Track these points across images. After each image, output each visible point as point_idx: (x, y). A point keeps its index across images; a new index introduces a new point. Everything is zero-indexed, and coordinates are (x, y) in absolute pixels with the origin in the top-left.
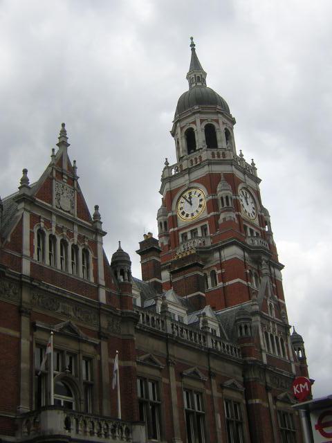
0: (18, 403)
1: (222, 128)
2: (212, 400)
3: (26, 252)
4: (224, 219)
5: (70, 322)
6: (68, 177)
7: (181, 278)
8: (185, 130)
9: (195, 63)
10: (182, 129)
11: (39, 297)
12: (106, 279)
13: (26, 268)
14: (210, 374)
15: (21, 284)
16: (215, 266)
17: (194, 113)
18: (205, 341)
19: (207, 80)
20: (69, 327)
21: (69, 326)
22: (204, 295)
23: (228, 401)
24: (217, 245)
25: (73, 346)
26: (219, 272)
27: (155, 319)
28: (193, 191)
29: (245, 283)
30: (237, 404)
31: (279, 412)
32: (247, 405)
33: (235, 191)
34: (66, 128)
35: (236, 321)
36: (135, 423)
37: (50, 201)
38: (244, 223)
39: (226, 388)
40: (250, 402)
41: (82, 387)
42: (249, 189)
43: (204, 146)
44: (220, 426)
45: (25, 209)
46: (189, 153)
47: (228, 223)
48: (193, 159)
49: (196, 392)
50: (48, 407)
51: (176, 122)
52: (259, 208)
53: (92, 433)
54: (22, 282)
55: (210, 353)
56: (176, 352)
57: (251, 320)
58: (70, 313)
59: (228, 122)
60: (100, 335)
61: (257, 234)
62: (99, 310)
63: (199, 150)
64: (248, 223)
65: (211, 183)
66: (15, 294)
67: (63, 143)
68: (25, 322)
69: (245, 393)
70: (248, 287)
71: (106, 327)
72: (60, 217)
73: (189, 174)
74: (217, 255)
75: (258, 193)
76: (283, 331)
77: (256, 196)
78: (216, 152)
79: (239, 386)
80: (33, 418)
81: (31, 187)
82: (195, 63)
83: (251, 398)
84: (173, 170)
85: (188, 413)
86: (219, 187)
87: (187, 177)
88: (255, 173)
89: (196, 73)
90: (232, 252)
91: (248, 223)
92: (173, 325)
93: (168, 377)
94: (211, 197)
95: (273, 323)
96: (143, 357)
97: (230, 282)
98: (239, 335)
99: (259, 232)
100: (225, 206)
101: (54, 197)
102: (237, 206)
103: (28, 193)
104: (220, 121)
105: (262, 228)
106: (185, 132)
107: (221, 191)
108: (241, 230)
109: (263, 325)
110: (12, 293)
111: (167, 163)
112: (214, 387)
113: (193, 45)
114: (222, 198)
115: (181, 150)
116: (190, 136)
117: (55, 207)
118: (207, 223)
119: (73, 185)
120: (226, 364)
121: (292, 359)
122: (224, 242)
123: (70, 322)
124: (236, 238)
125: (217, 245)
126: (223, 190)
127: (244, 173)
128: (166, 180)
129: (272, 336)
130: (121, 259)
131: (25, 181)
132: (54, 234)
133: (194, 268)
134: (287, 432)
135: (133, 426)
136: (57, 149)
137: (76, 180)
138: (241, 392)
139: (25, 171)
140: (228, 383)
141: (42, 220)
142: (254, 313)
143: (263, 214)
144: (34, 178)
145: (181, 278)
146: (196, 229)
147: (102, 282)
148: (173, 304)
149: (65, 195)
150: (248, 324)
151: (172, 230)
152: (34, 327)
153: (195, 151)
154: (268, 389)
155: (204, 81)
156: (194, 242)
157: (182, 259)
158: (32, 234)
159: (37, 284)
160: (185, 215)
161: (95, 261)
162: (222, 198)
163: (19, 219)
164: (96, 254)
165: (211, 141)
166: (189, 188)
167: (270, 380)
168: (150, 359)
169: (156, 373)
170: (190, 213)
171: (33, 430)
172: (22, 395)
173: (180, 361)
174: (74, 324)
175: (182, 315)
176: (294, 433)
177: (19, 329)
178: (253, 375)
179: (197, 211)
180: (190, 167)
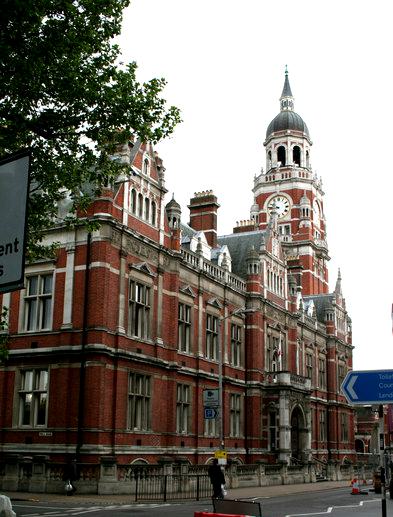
2: (119, 281)
3: (266, 285)
28: (281, 198)
30: (239, 327)
49: (138, 284)
65: (296, 195)
74: (295, 250)
77: (321, 206)
86: (302, 201)
126: (305, 204)
130: (172, 207)
150: (177, 217)
152: (268, 326)
178: (256, 306)
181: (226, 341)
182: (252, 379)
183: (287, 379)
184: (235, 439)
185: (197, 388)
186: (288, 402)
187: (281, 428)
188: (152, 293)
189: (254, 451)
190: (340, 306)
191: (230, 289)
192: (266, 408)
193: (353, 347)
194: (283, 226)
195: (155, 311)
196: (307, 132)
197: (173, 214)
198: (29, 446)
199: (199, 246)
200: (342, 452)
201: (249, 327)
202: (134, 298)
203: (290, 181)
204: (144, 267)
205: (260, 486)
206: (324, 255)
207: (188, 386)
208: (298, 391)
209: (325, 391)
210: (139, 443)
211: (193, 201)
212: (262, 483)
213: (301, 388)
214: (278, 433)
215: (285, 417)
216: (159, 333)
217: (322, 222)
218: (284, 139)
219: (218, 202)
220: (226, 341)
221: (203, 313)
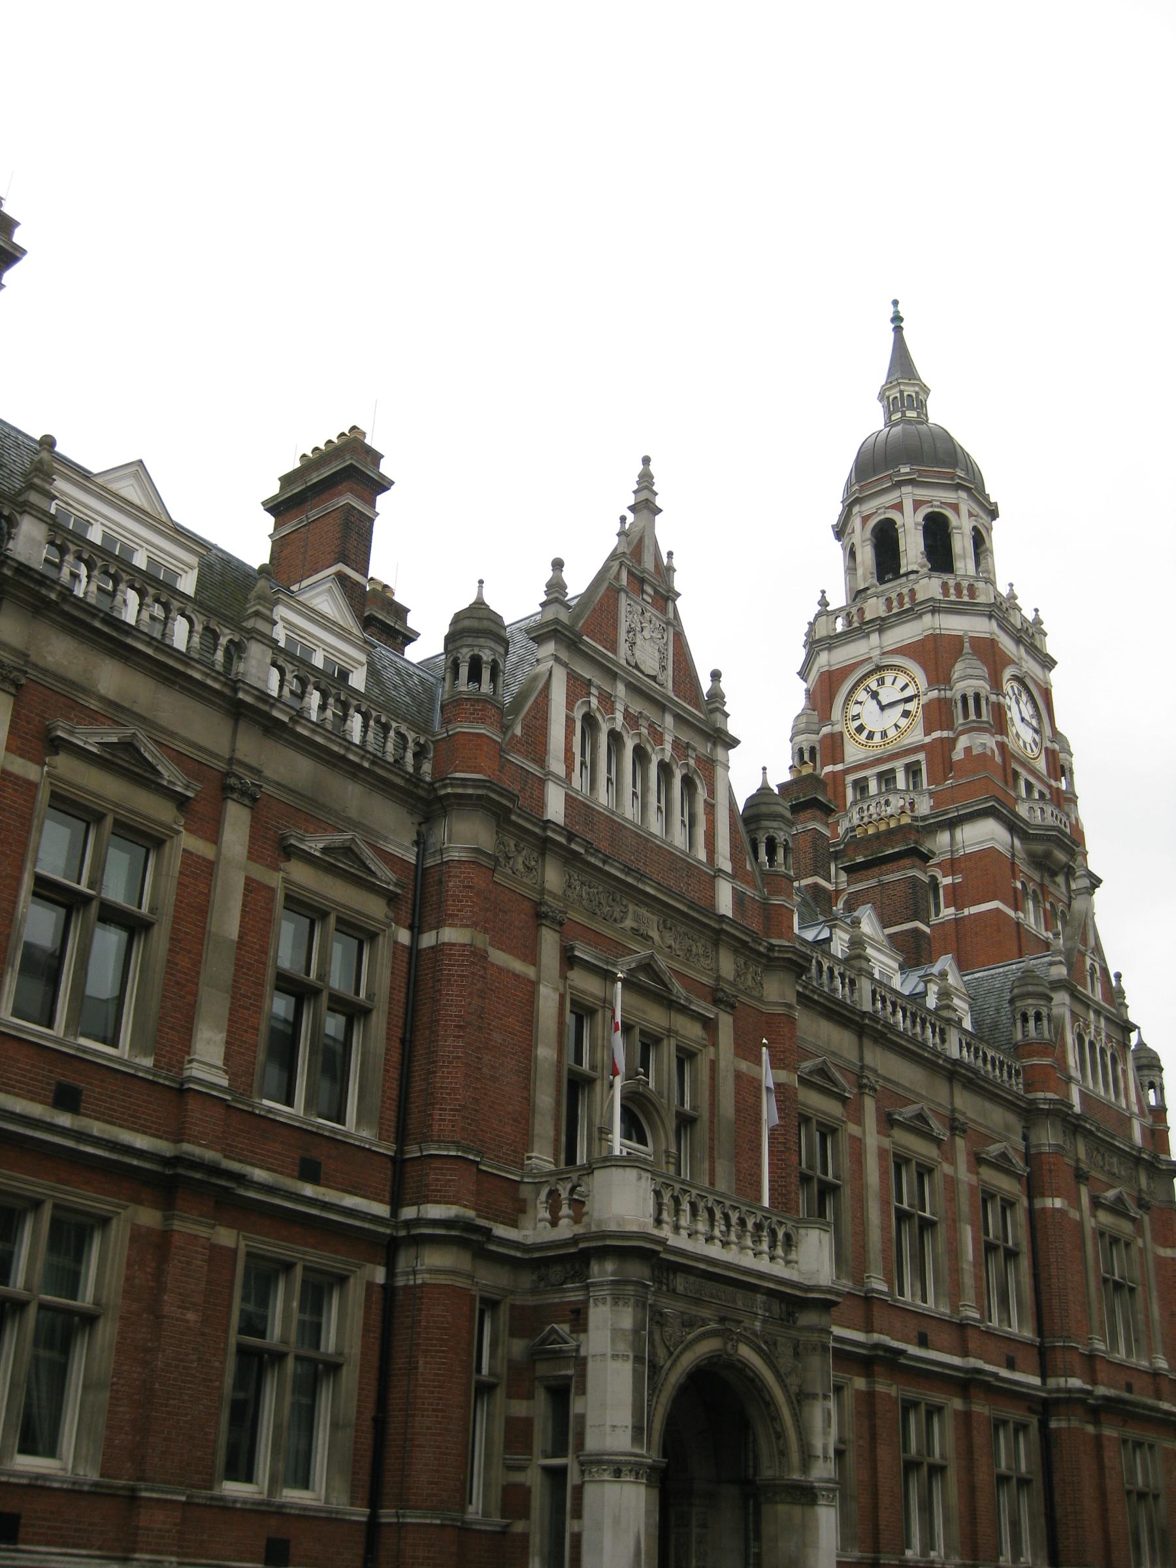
0: (527, 1146)
3: (557, 766)
4: (968, 750)
5: (652, 956)
6: (656, 591)
7: (873, 882)
8: (872, 523)
10: (865, 520)
11: (583, 883)
12: (733, 859)
13: (555, 808)
14: (956, 1126)
15: (544, 846)
16: (938, 865)
17: (899, 485)
19: (931, 404)
21: (649, 965)
22: (927, 930)
24: (946, 812)
25: (655, 1017)
26: (948, 880)
27: (836, 973)
28: (889, 677)
29: (1011, 913)
30: (1008, 1204)
31: (1102, 1234)
32: (1031, 1212)
33: (996, 685)
34: (653, 468)
35: (1012, 1001)
36: (800, 1223)
37: (613, 647)
38: (1015, 766)
40: (428, 940)
41: (671, 1124)
42: (1028, 681)
43: (922, 566)
44: (970, 1257)
45: (557, 659)
46: (881, 580)
48: (894, 596)
50: (610, 1162)
51: (851, 503)
52: (1048, 731)
53: (710, 1239)
54: (548, 840)
55: (953, 1073)
56: (879, 1060)
57: (1052, 999)
58: (651, 933)
59: (982, 514)
60: (717, 998)
61: (1042, 795)
62: (716, 933)
63: (907, 574)
64: (1024, 765)
65: (936, 656)
66: (529, 869)
67: (645, 505)
68: (549, 942)
69: (1028, 1178)
70: (1018, 924)
71: (731, 978)
72: (635, 689)
73: (881, 631)
74: (944, 838)
75: (1047, 694)
76: (1117, 1035)
78: (952, 583)
79: (1018, 1161)
80: (569, 1186)
81: (573, 603)
83: (1043, 1195)
84: (840, 621)
86: (959, 669)
87: (874, 638)
88: (1043, 642)
89: (903, 382)
90: (983, 834)
91: (1024, 765)
92: (874, 992)
93: (859, 1122)
94: (934, 694)
95: (1098, 1013)
96: (807, 1065)
97: (974, 910)
98: (1019, 1036)
99: (1046, 792)
100: (973, 717)
101: (623, 635)
102: (1000, 723)
103: (564, 617)
104: (964, 509)
105: (1053, 783)
106: (880, 521)
107: (963, 678)
108: (1006, 783)
109: (1075, 1016)
110: (520, 867)
111: (824, 603)
112: (962, 1158)
113: (897, 319)
114: (964, 698)
115: (860, 572)
116: (886, 540)
117: (623, 662)
118: (921, 756)
119: (664, 611)
120: (988, 1105)
121: (1135, 1109)
122: (965, 807)
123: (652, 956)
124: (998, 800)
125: (946, 812)
126: (968, 679)
127: (1018, 641)
128: (815, 644)
129: (1092, 1044)
131: (556, 587)
132: (618, 729)
133: (907, 862)
134: (1118, 1286)
135: (802, 1231)
136: (630, 517)
137: (674, 601)
138: (1018, 1177)
139: (558, 565)
140: (994, 1149)
141: (594, 691)
142: (1058, 985)
143: (1057, 747)
144: (577, 584)
145: (873, 882)
146: (893, 770)
147: (727, 866)
149: (646, 634)
151: (828, 769)
152: (569, 960)
153: (897, 575)
154: (1080, 1176)
155: (922, 406)
156: (887, 803)
157: (878, 835)
158: (570, 721)
159: (582, 851)
160: (865, 733)
161: (710, 808)
162: (964, 698)
163: (541, 685)
164: (712, 792)
165: (939, 553)
166: (879, 668)
167: (1087, 1154)
168: (822, 1071)
169: (833, 1108)
170: (869, 728)
171: (568, 1216)
172: (538, 1129)
173: (890, 1086)
174: (662, 963)
175: (889, 972)
176: (1132, 1290)
177: (533, 958)
178: (464, 836)
179: (896, 726)
180: (883, 615)
182: (421, 1199)
183: (624, 1201)
186: (627, 1320)
188: (845, 1145)
194: (899, 765)
201: (428, 940)
202: (811, 1166)
203: (912, 612)
204: (920, 1117)
206: (1061, 856)
207: (940, 1409)
209: (1028, 1334)
214: (579, 1490)
215: (612, 1406)
217: (1051, 755)
219: (385, 468)
221: (882, 1153)
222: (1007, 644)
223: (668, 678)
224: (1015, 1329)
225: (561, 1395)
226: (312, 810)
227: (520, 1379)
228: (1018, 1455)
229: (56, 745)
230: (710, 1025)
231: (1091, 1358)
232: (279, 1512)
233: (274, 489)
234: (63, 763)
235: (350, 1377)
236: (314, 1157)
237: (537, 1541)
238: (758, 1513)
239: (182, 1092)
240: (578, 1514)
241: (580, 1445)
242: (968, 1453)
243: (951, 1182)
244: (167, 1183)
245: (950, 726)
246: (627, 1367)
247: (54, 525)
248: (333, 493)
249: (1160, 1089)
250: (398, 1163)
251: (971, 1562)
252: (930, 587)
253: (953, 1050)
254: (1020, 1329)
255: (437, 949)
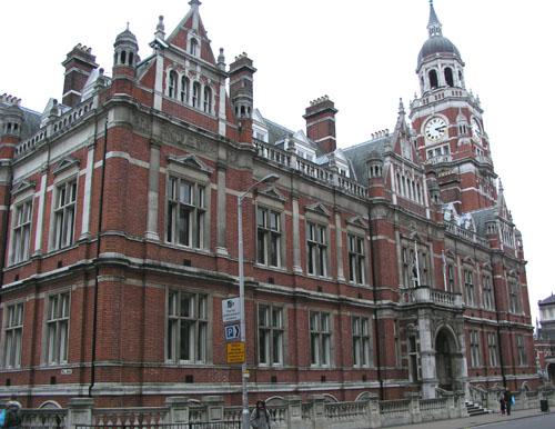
1: (457, 70)
9: (433, 17)
13: (158, 104)
14: (335, 210)
15: (152, 117)
18: (289, 162)
20: (191, 160)
23: (352, 236)
39: (263, 195)
40: (374, 238)
47: (464, 146)
49: (319, 225)
51: (420, 66)
55: (335, 192)
56: (461, 247)
62: (218, 142)
65: (451, 114)
68: (397, 233)
72: (406, 164)
75: (481, 121)
77: (480, 123)
82: (433, 17)
85: (351, 256)
87: (432, 108)
90: (468, 168)
116: (433, 75)
126: (461, 121)
131: (160, 28)
142: (497, 217)
144: (169, 30)
147: (224, 117)
148: (300, 142)
152: (401, 237)
154: (504, 268)
158: (165, 74)
164: (218, 92)
178: (379, 213)
181: (340, 254)
182: (381, 299)
183: (425, 295)
184: (362, 370)
185: (482, 332)
186: (428, 322)
187: (422, 354)
189: (388, 383)
190: (505, 218)
191: (341, 194)
192: (405, 331)
193: (64, 64)
194: (442, 146)
195: (214, 214)
196: (457, 53)
197: (240, 103)
198: (53, 387)
199: (452, 217)
200: (519, 377)
201: (374, 238)
203: (444, 101)
205: (449, 418)
207: (367, 319)
208: (444, 309)
210: (189, 379)
211: (308, 110)
212: (452, 416)
213: (449, 305)
216: (220, 240)
217: (484, 140)
218: (434, 63)
219: (336, 107)
220: (340, 254)
222: (471, 108)
223: (412, 159)
224: (363, 284)
225: (413, 339)
226: (350, 212)
227: (403, 336)
228: (492, 340)
229: (169, 161)
230: (428, 247)
231: (509, 314)
232: (273, 370)
233: (304, 113)
234: (171, 167)
235: (371, 339)
236: (361, 293)
237: (410, 371)
238: (450, 362)
239: (338, 284)
240: (420, 364)
241: (419, 350)
242: (339, 328)
243: (476, 275)
244: (339, 304)
245: (456, 135)
246: (429, 333)
247: (297, 157)
248: (321, 115)
249: (521, 241)
250: (374, 291)
251: (293, 367)
252: (448, 93)
253: (475, 240)
254: (491, 309)
255: (377, 241)
